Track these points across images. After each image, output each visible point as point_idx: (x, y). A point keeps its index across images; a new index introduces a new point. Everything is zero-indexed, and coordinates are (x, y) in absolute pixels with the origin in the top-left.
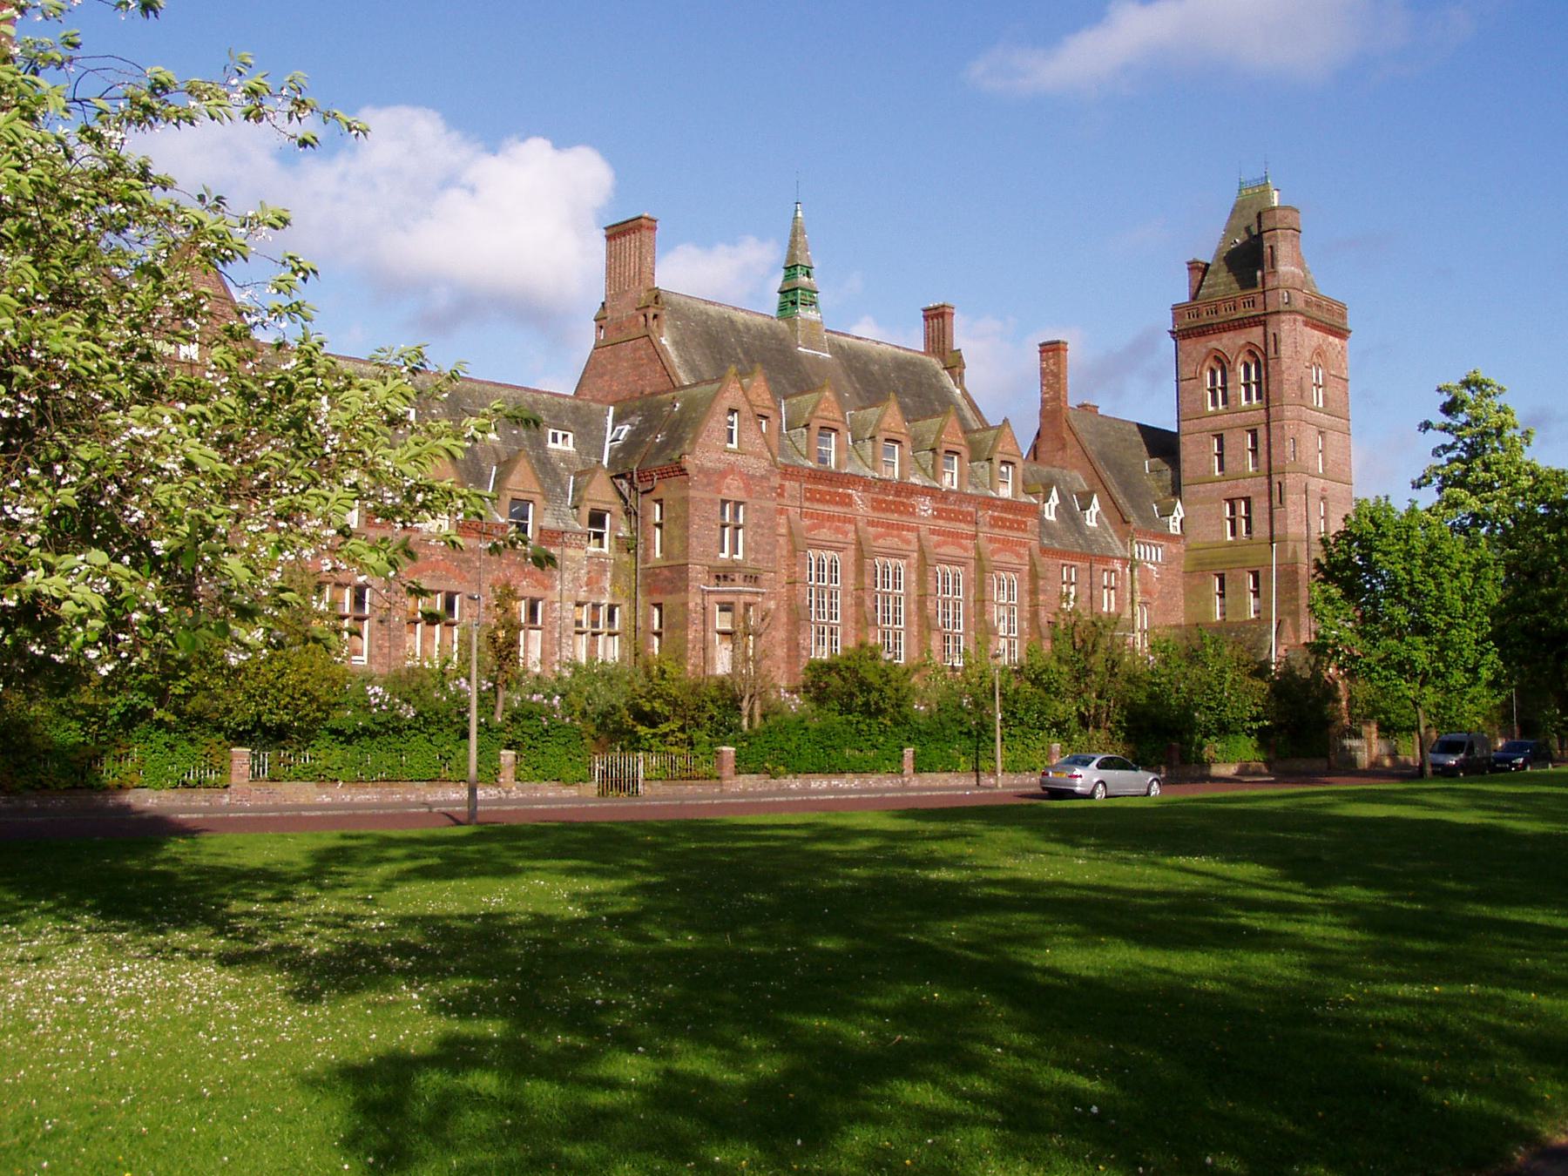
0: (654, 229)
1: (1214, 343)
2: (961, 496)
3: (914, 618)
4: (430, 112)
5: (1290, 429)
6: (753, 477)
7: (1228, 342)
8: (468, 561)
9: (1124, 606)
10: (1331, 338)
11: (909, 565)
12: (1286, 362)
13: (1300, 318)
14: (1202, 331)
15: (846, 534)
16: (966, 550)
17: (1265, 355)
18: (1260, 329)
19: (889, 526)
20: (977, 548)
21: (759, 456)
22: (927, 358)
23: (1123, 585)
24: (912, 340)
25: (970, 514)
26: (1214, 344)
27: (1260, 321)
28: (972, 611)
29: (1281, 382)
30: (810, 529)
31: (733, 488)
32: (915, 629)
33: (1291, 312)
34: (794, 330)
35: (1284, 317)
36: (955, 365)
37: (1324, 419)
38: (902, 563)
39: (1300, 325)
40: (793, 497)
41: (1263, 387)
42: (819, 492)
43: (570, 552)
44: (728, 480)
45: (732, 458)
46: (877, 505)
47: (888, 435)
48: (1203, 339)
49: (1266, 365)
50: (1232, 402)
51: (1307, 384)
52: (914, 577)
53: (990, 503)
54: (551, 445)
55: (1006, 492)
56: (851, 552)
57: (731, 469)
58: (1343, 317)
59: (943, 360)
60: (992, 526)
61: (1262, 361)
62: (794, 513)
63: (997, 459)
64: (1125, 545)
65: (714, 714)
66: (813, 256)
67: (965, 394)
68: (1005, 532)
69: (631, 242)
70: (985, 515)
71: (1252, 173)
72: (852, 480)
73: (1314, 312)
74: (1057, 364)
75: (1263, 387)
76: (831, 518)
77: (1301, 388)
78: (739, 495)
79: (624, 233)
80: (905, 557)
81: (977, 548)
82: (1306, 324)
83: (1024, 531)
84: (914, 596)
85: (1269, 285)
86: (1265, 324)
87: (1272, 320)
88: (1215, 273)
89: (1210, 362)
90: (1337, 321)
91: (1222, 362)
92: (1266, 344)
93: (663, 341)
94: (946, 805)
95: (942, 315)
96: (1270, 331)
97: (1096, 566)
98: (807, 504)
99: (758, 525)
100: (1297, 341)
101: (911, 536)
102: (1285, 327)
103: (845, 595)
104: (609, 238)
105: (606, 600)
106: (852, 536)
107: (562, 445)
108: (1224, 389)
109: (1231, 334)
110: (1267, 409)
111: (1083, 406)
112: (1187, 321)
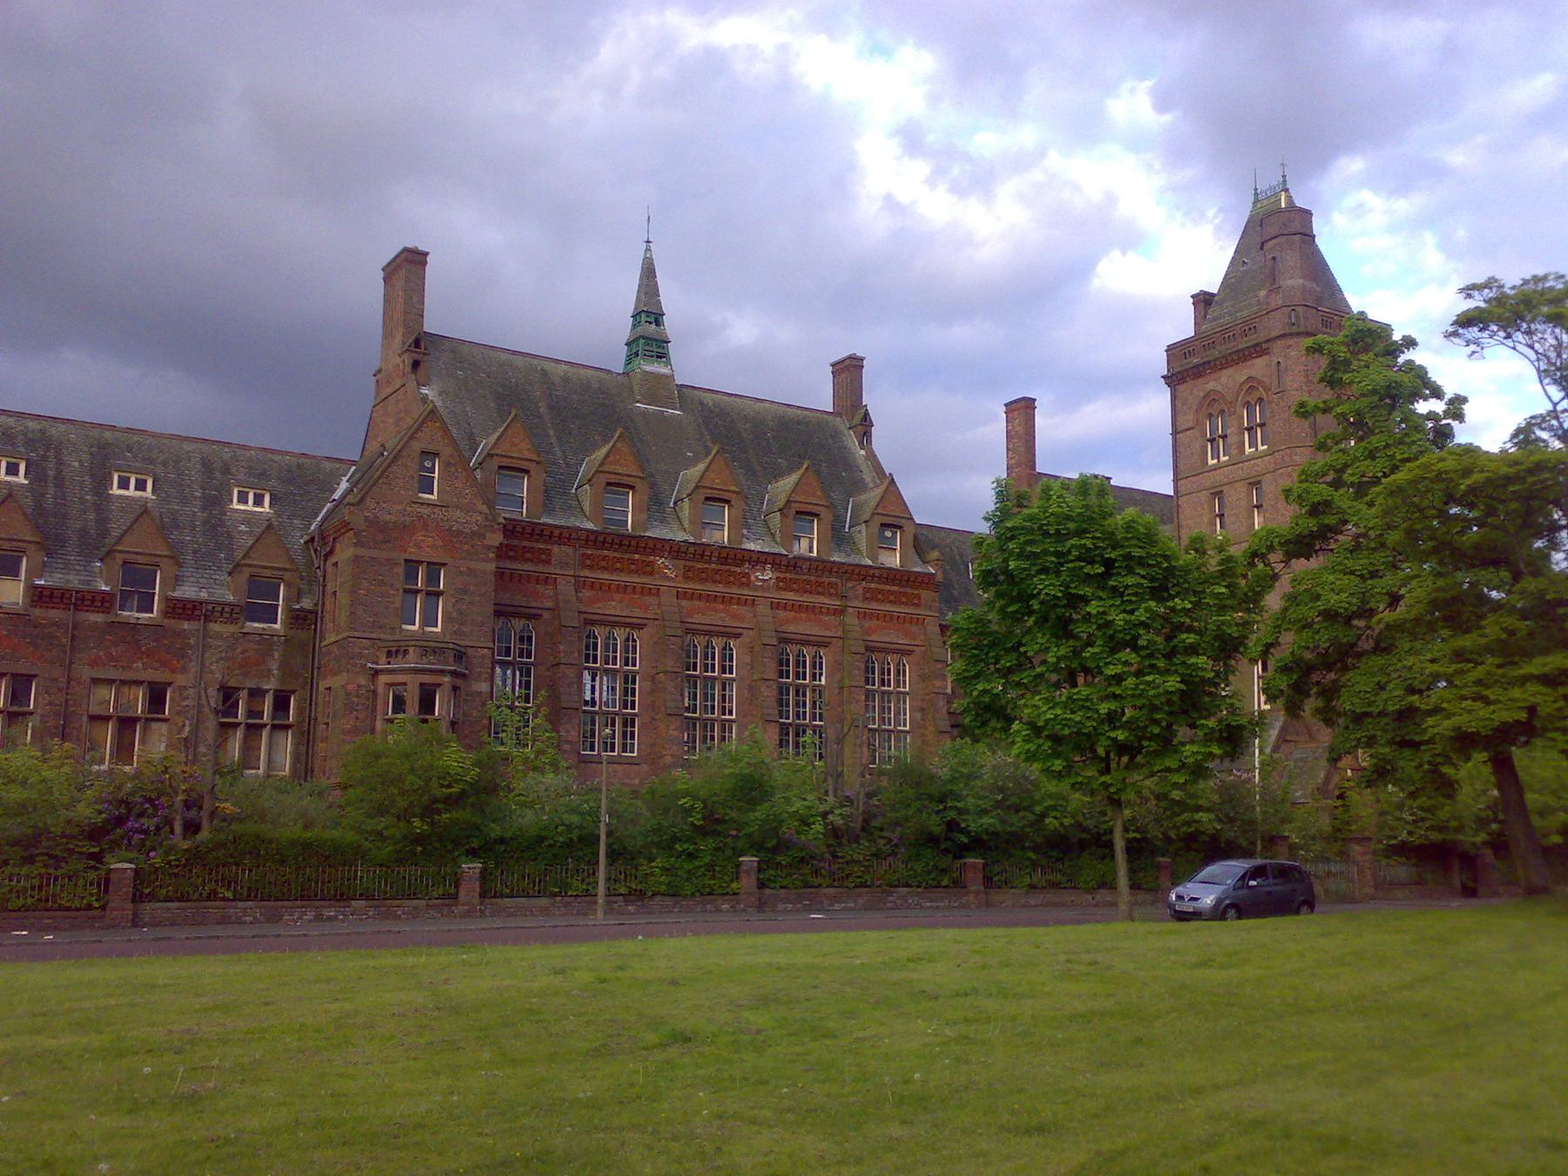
1: (1212, 384)
2: (820, 566)
6: (460, 533)
14: (1198, 372)
15: (646, 608)
24: (821, 396)
26: (1211, 385)
31: (426, 547)
36: (864, 426)
42: (604, 558)
46: (688, 574)
48: (1201, 380)
54: (116, 491)
55: (894, 560)
66: (670, 298)
67: (871, 456)
71: (1268, 181)
72: (659, 546)
78: (428, 555)
83: (918, 605)
88: (1220, 303)
94: (298, 919)
98: (586, 573)
105: (271, 685)
109: (1230, 371)
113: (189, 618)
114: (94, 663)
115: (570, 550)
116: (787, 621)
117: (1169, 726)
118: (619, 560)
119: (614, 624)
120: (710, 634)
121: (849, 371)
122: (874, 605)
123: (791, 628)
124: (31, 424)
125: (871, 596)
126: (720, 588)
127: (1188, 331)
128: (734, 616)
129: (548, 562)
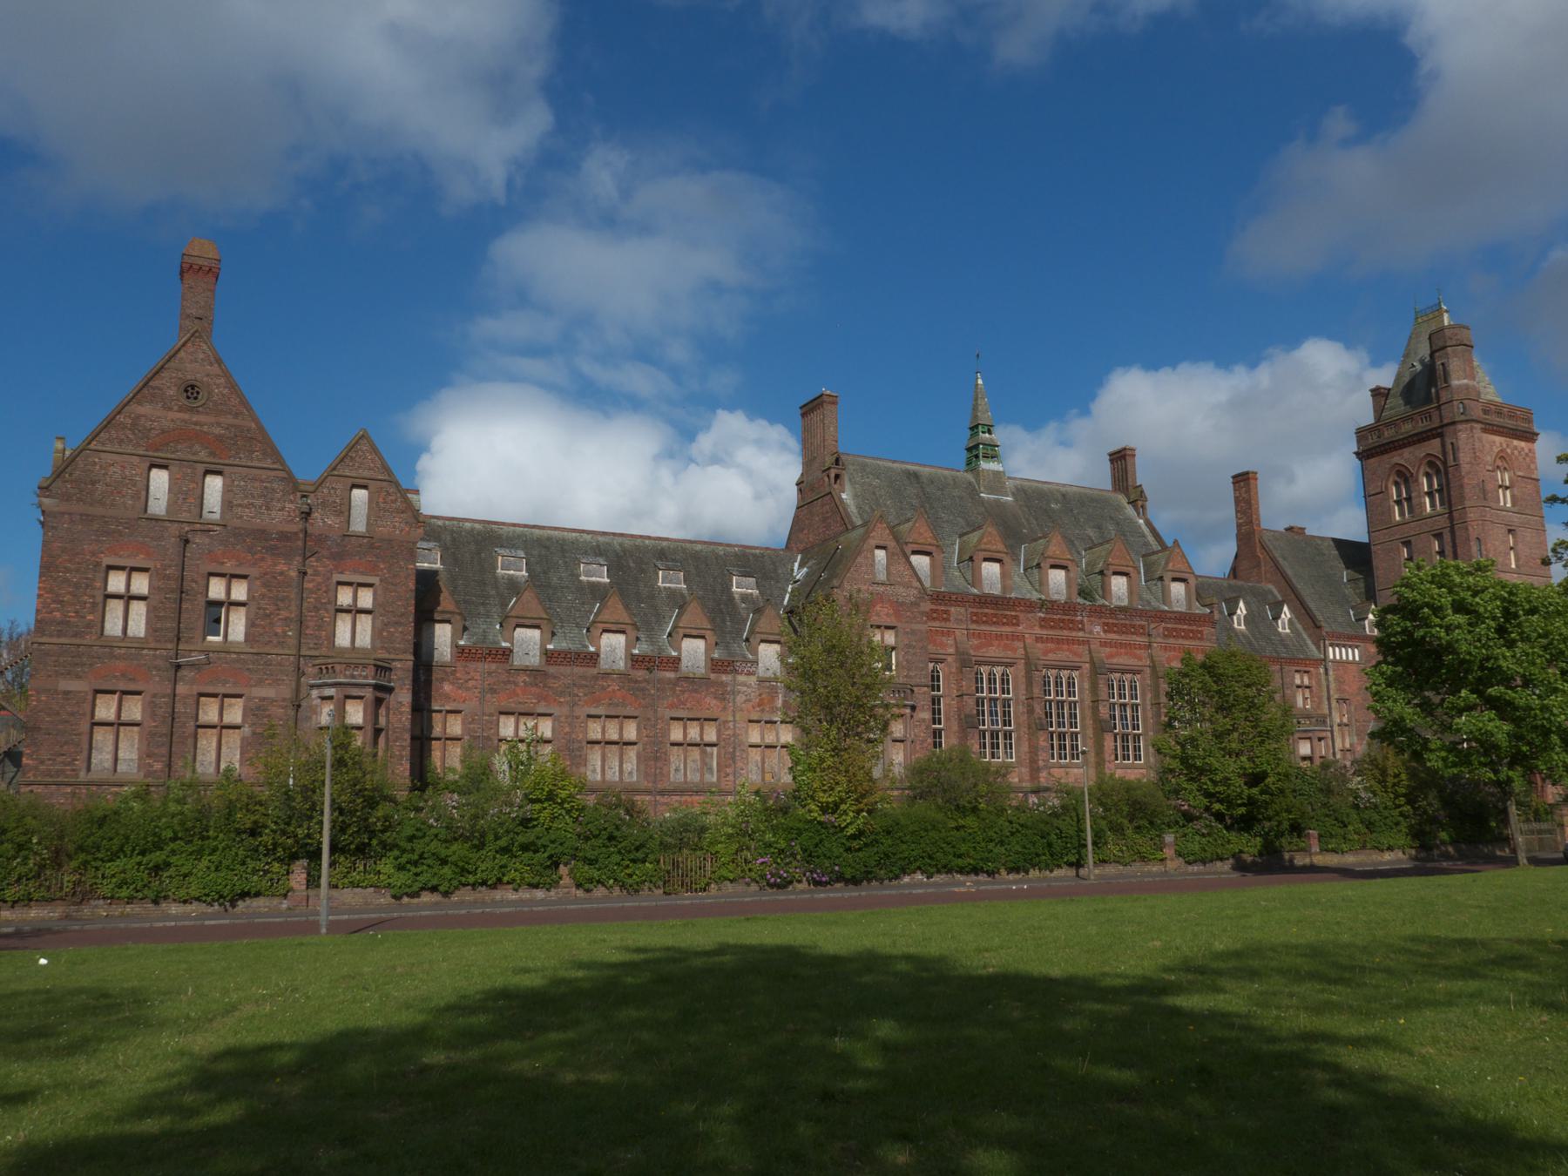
0: (834, 403)
3: (1089, 722)
4: (1184, 367)
5: (1474, 530)
6: (902, 604)
7: (1406, 457)
8: (643, 690)
9: (1320, 703)
10: (1516, 442)
11: (1143, 679)
12: (1465, 468)
13: (1478, 426)
15: (1015, 650)
16: (1140, 659)
17: (1445, 463)
18: (1438, 441)
19: (1059, 641)
20: (1151, 657)
21: (908, 586)
22: (1113, 495)
23: (1319, 683)
24: (1100, 478)
25: (1143, 627)
26: (1396, 459)
27: (1437, 433)
28: (1150, 714)
29: (1462, 486)
30: (978, 648)
32: (1090, 732)
33: (1467, 421)
34: (977, 476)
35: (1460, 427)
36: (1138, 500)
37: (1516, 519)
38: (1075, 674)
39: (1478, 433)
40: (959, 621)
41: (1447, 493)
42: (986, 615)
43: (741, 678)
44: (878, 608)
45: (881, 589)
46: (1108, 628)
47: (1052, 561)
49: (1446, 473)
50: (1417, 511)
51: (1489, 487)
52: (1086, 685)
53: (1161, 616)
56: (1021, 665)
57: (881, 598)
58: (1530, 421)
59: (1128, 496)
60: (1165, 636)
61: (1442, 468)
62: (960, 634)
63: (1168, 576)
64: (1318, 648)
65: (962, 829)
67: (1148, 524)
68: (1180, 641)
69: (815, 417)
70: (1157, 629)
73: (1497, 420)
74: (1248, 491)
75: (1447, 493)
76: (999, 637)
77: (1484, 491)
79: (812, 410)
80: (1077, 668)
81: (1151, 657)
82: (1485, 431)
83: (1201, 639)
84: (1088, 702)
85: (1443, 400)
86: (1441, 435)
87: (1448, 431)
89: (1393, 477)
90: (1523, 425)
91: (1404, 477)
92: (1444, 453)
93: (844, 496)
95: (1124, 457)
96: (1448, 441)
97: (1286, 668)
98: (974, 626)
99: (909, 646)
100: (1478, 449)
101: (1082, 649)
102: (1463, 436)
103: (1017, 704)
104: (804, 415)
106: (1021, 651)
107: (741, 587)
108: (1409, 499)
110: (1451, 513)
111: (1290, 529)
112: (1373, 440)
113: (725, 672)
114: (671, 706)
115: (962, 610)
116: (1111, 656)
117: (664, 846)
118: (995, 615)
119: (994, 664)
120: (1123, 672)
121: (1121, 459)
122: (1172, 641)
123: (1115, 661)
124: (601, 539)
125: (1169, 634)
126: (1066, 633)
127: (1368, 418)
128: (1075, 654)
129: (947, 620)
